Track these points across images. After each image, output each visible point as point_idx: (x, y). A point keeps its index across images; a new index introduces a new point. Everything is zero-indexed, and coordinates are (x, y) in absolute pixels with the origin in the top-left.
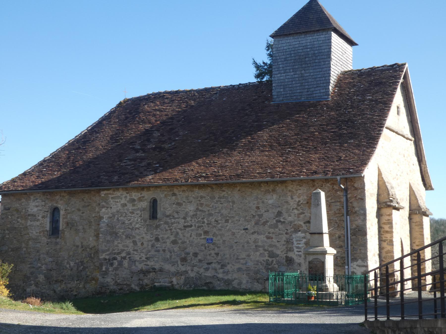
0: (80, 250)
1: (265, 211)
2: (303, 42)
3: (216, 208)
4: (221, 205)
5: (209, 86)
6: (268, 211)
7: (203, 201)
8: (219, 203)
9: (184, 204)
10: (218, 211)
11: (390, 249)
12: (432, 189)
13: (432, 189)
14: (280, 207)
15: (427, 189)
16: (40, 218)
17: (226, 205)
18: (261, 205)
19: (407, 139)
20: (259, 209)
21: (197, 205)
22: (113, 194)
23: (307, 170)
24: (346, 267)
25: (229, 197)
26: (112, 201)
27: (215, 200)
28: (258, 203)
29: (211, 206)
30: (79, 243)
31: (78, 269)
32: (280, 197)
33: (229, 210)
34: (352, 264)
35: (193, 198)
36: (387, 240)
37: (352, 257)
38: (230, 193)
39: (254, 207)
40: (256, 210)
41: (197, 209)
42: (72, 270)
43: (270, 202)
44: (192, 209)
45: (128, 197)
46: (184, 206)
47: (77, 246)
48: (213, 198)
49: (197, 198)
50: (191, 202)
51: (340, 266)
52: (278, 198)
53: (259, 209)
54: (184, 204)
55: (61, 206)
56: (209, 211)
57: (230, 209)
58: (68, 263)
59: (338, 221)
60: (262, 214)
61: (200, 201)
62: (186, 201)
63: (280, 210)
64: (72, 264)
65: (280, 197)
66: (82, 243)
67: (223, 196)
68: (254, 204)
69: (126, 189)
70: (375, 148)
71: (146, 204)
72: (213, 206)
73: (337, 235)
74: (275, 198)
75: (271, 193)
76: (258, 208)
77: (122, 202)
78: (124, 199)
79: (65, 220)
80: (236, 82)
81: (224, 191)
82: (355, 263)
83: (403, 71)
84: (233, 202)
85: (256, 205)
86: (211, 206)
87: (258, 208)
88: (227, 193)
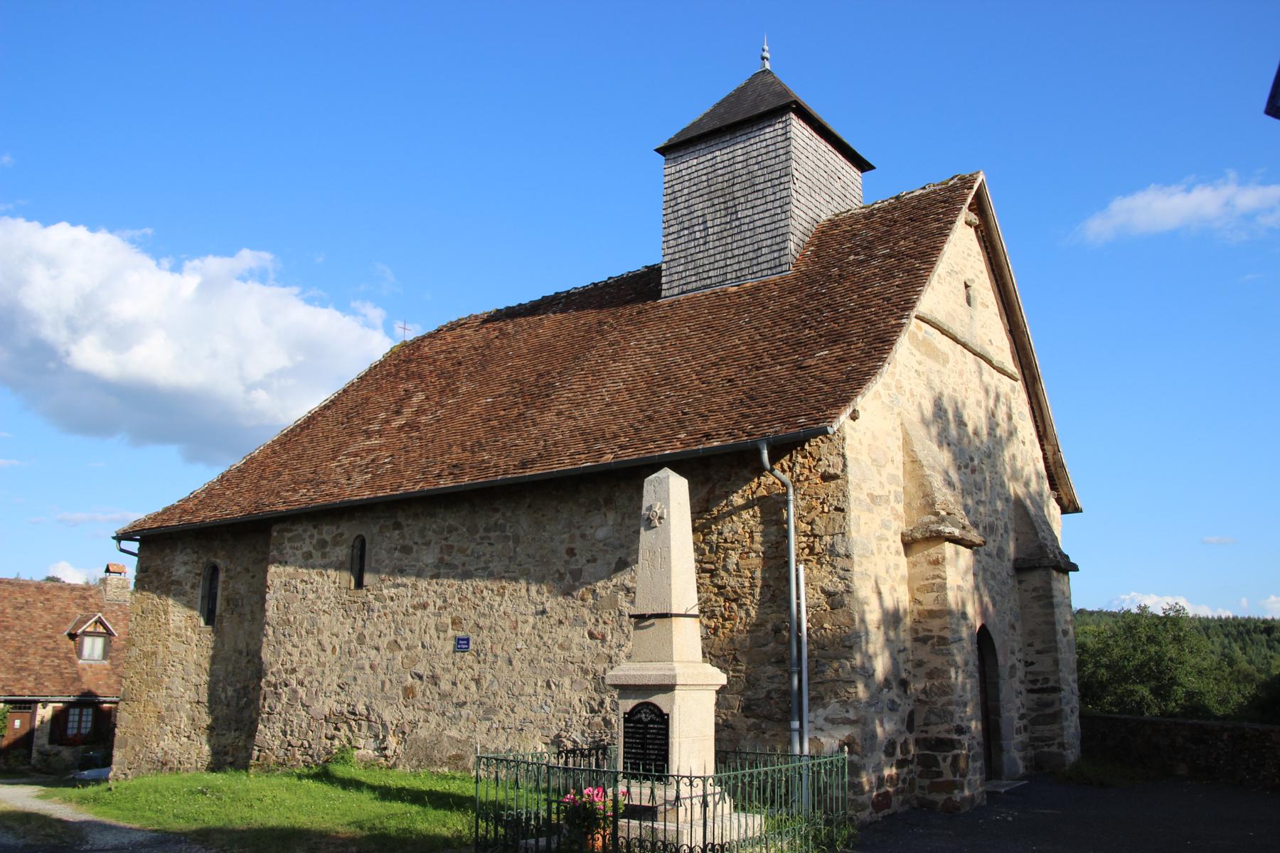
0: (244, 661)
1: (588, 561)
2: (726, 157)
3: (478, 557)
4: (489, 549)
5: (550, 292)
6: (594, 560)
7: (453, 540)
8: (486, 542)
9: (415, 547)
10: (482, 565)
11: (939, 666)
12: (1077, 510)
13: (1077, 510)
14: (622, 546)
15: (1064, 511)
16: (188, 588)
17: (500, 547)
18: (578, 545)
19: (1002, 371)
20: (575, 555)
21: (441, 552)
22: (291, 531)
23: (689, 434)
24: (796, 724)
25: (508, 525)
26: (290, 552)
27: (477, 536)
28: (572, 538)
29: (469, 552)
30: (242, 646)
31: (237, 704)
32: (623, 519)
33: (507, 562)
34: (812, 714)
35: (434, 531)
36: (932, 637)
37: (813, 693)
38: (509, 514)
39: (562, 549)
40: (566, 557)
41: (441, 560)
42: (228, 705)
43: (601, 533)
44: (430, 561)
45: (316, 536)
46: (414, 555)
47: (241, 653)
48: (473, 530)
49: (442, 533)
50: (428, 544)
51: (779, 721)
52: (619, 520)
53: (575, 555)
54: (415, 547)
55: (220, 562)
56: (464, 565)
57: (510, 558)
58: (224, 690)
59: (771, 583)
60: (581, 570)
61: (446, 539)
62: (420, 541)
63: (623, 556)
64: (230, 692)
65: (623, 519)
66: (248, 645)
67: (496, 524)
68: (562, 542)
69: (977, 588)
70: (883, 360)
71: (345, 551)
72: (473, 552)
73: (769, 626)
74: (611, 523)
75: (604, 510)
76: (571, 552)
77: (305, 550)
78: (308, 541)
79: (225, 593)
80: (601, 277)
81: (496, 510)
82: (820, 711)
83: (971, 188)
84: (517, 540)
85: (566, 546)
86: (469, 552)
87: (571, 552)
88: (504, 515)
